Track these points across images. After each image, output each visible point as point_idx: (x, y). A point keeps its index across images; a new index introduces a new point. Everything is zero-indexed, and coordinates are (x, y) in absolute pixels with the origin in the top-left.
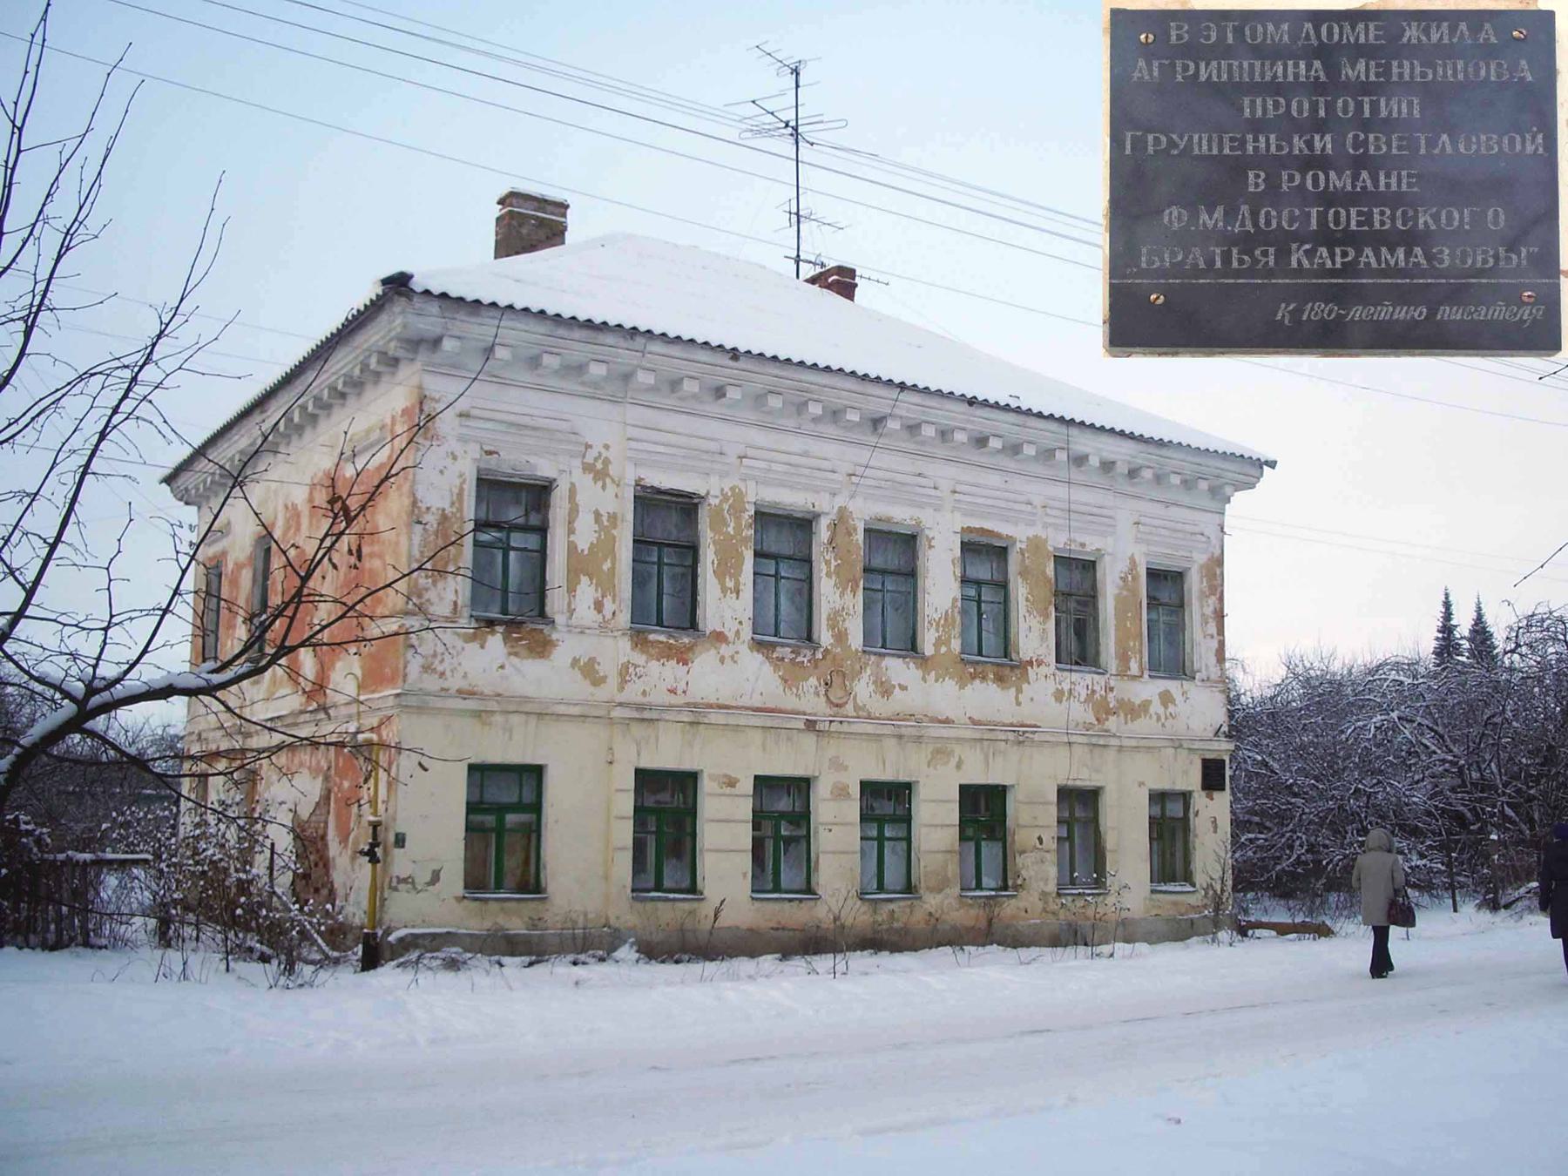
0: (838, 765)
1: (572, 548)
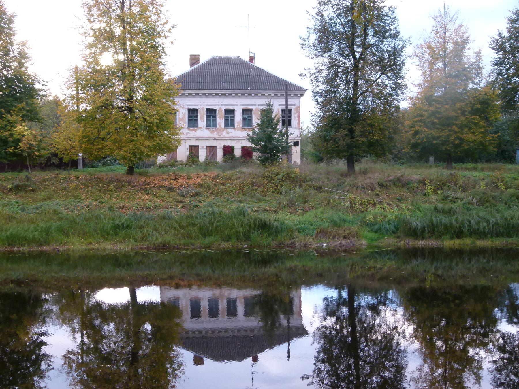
0: (220, 144)
1: (179, 118)
